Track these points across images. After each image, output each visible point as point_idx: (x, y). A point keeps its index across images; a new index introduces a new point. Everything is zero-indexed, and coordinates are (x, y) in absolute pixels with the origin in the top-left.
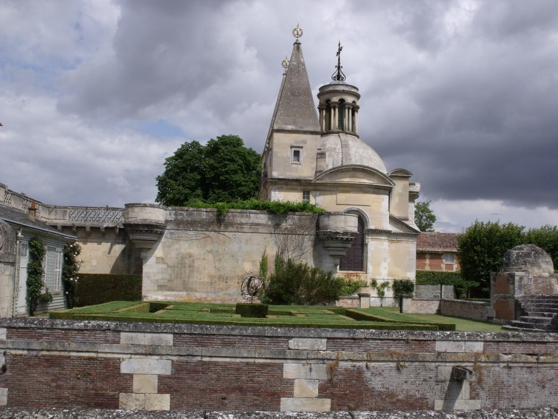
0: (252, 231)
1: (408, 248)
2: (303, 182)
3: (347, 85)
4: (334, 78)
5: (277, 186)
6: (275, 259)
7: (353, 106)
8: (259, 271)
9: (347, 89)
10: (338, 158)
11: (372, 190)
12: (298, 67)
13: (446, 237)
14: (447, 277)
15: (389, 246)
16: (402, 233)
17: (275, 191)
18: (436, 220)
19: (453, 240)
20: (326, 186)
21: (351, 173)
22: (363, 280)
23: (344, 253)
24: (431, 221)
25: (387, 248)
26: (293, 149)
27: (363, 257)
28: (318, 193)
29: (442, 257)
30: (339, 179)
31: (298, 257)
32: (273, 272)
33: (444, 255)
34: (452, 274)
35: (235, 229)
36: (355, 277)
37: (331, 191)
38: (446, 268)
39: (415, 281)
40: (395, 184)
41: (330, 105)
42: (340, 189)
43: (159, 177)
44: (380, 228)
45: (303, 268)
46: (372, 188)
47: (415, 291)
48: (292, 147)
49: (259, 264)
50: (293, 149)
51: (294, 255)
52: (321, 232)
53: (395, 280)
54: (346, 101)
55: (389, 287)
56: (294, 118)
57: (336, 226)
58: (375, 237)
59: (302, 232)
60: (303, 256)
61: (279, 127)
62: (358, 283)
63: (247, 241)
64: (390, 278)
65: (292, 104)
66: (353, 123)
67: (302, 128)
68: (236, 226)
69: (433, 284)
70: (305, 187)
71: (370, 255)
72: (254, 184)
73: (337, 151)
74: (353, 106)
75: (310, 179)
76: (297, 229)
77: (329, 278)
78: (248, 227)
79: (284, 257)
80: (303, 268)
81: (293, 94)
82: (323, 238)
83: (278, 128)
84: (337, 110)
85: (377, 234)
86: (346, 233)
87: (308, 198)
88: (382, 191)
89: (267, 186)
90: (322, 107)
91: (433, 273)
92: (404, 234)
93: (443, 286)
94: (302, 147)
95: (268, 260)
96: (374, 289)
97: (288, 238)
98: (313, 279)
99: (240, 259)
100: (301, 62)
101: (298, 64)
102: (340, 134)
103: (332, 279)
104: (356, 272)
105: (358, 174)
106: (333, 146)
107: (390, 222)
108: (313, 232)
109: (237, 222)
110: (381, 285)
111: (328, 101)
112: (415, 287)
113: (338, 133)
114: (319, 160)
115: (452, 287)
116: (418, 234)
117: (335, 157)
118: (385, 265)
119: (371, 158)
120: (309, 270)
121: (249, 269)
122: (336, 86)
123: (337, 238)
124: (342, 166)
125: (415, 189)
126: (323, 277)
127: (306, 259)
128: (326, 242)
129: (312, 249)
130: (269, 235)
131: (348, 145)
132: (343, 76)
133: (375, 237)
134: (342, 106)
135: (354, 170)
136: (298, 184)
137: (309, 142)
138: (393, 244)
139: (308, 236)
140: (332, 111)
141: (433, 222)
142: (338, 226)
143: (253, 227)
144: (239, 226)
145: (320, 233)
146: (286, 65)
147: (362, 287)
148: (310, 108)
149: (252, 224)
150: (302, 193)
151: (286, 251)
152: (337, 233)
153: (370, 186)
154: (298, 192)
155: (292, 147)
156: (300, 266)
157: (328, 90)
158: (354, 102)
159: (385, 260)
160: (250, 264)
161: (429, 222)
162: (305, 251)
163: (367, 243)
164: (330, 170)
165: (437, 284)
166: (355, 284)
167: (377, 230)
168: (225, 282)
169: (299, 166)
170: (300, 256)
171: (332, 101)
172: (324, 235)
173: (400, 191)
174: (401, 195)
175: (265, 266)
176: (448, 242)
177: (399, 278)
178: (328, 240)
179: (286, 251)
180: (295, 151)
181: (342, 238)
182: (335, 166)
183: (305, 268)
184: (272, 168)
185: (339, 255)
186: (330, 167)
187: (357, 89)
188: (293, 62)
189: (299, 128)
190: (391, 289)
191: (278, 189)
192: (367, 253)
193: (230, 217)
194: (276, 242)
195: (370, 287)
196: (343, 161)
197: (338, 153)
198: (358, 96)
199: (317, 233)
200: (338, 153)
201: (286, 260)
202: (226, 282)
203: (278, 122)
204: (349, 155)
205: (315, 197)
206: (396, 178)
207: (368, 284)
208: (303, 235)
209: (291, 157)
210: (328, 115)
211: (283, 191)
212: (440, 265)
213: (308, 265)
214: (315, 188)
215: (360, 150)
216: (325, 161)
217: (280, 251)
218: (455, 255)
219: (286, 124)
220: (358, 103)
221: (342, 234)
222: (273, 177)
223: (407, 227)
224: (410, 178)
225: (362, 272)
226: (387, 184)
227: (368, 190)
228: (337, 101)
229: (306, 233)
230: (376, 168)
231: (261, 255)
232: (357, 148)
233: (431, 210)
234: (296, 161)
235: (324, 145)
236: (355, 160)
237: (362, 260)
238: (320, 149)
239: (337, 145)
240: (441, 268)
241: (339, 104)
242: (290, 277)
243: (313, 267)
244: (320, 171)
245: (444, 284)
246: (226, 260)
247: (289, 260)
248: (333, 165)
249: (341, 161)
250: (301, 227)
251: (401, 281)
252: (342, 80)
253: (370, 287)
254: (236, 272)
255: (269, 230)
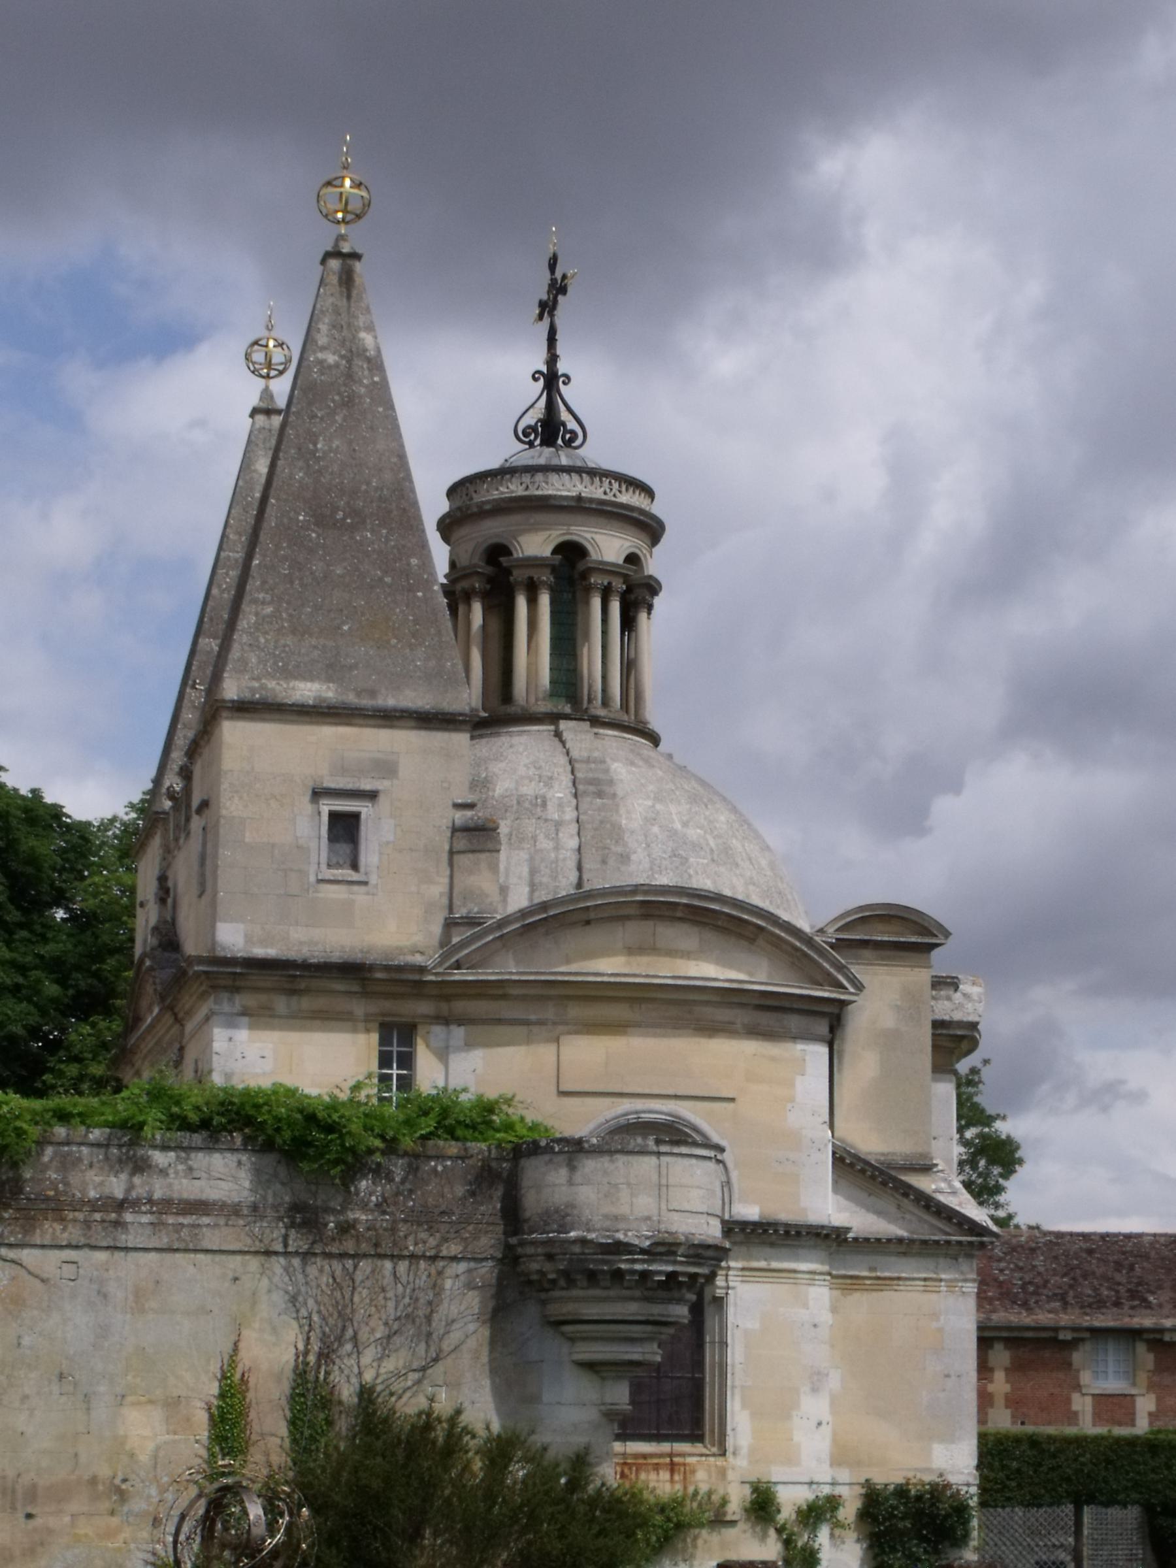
0: (164, 1241)
1: (935, 1316)
2: (379, 975)
3: (595, 473)
4: (525, 435)
5: (240, 1001)
6: (286, 1387)
7: (626, 578)
8: (204, 1453)
9: (594, 491)
10: (557, 848)
11: (742, 1017)
12: (350, 376)
13: (1090, 1252)
14: (1109, 1462)
15: (834, 1310)
16: (900, 1240)
17: (231, 1025)
18: (1020, 1161)
19: (1131, 1268)
20: (504, 997)
21: (634, 931)
22: (704, 1488)
23: (653, 1353)
24: (996, 1170)
25: (826, 1317)
26: (327, 806)
27: (702, 1371)
28: (458, 1033)
29: (1077, 1357)
30: (568, 961)
31: (415, 1376)
32: (280, 1458)
33: (1088, 1346)
34: (1132, 1442)
35: (74, 1233)
36: (665, 1475)
37: (526, 1023)
38: (1098, 1417)
39: (974, 1490)
40: (859, 987)
41: (508, 572)
42: (575, 1011)
43: (482, 1095)
44: (785, 1215)
45: (439, 1434)
46: (742, 1005)
47: (974, 1543)
48: (318, 794)
49: (202, 1417)
50: (327, 806)
51: (389, 1365)
52: (534, 1243)
53: (868, 1483)
54: (594, 555)
55: (837, 1525)
56: (331, 643)
57: (614, 1210)
58: (762, 1264)
59: (432, 1242)
60: (437, 1371)
61: (253, 690)
62: (677, 1503)
63: (139, 1295)
64: (844, 1475)
65: (318, 567)
66: (630, 666)
67: (373, 693)
68: (80, 1216)
69: (1034, 1502)
70: (387, 1005)
71: (736, 1354)
72: (62, 982)
73: (553, 813)
74: (626, 578)
75: (418, 959)
76: (403, 1229)
77: (575, 1484)
78: (145, 1219)
79: (335, 1377)
80: (439, 1434)
81: (322, 520)
82: (542, 1273)
83: (247, 695)
84: (545, 600)
85: (772, 1245)
86: (664, 1248)
87: (407, 1061)
88: (794, 1022)
89: (186, 1002)
90: (464, 584)
91: (1033, 1442)
92: (912, 1241)
93: (1088, 1512)
94: (372, 796)
95: (250, 1395)
96: (764, 1537)
97: (359, 1276)
98: (492, 1489)
99: (102, 1389)
100: (362, 353)
101: (349, 361)
102: (563, 725)
103: (591, 1489)
104: (665, 1447)
105: (668, 933)
106: (529, 790)
107: (835, 1182)
108: (488, 1242)
109: (84, 1191)
110: (799, 1512)
111: (497, 552)
112: (975, 1523)
113: (554, 718)
114: (463, 860)
115: (1129, 1516)
116: (982, 1245)
117: (545, 844)
118: (815, 1406)
119: (726, 850)
120: (473, 1444)
121: (150, 1446)
122: (539, 477)
123: (618, 1275)
124: (581, 893)
125: (961, 1006)
126: (543, 1472)
127: (453, 1385)
128: (557, 1293)
129: (486, 1332)
130: (254, 1263)
131: (611, 782)
132: (572, 425)
133: (762, 1264)
134: (571, 582)
135: (646, 917)
136: (355, 988)
137: (406, 768)
138: (857, 1295)
139: (462, 1267)
140: (521, 604)
141: (1008, 1172)
142: (624, 1209)
143: (171, 1220)
144: (98, 1216)
145: (530, 1250)
146: (269, 365)
147: (701, 1525)
148: (411, 589)
149: (166, 1205)
150: (375, 1037)
151: (348, 1347)
152: (620, 1248)
153: (732, 996)
154: (355, 1030)
155: (318, 794)
156: (426, 1423)
157: (495, 495)
158: (632, 559)
159: (816, 1380)
160: (157, 1414)
161: (985, 1175)
162: (446, 1346)
163: (719, 1292)
164: (523, 913)
165: (1056, 1502)
166: (662, 1510)
167: (774, 1225)
168: (21, 1516)
169: (360, 896)
170: (423, 1369)
171: (518, 554)
172: (550, 1257)
173: (889, 1021)
174: (889, 1041)
175: (234, 1425)
176: (1105, 1278)
177: (888, 1476)
178: (571, 1283)
179: (348, 1347)
180: (334, 816)
181: (645, 1275)
182: (543, 896)
183: (450, 1435)
184: (213, 904)
185: (632, 1363)
186: (519, 900)
187: (648, 492)
188: (323, 349)
189: (359, 694)
190: (851, 1536)
191: (245, 1013)
192: (724, 1344)
193: (46, 1167)
194: (293, 1299)
195: (741, 1526)
196: (586, 866)
197: (558, 825)
198: (652, 530)
199: (508, 1247)
200: (558, 825)
201: (347, 1393)
202: (29, 1516)
203: (244, 661)
204: (617, 833)
205: (443, 1055)
206: (867, 953)
207: (734, 1508)
208: (434, 1258)
209: (313, 845)
210: (495, 626)
211: (272, 1028)
212: (1068, 1401)
213: (464, 1419)
214: (444, 1007)
215: (673, 809)
216: (494, 868)
217: (315, 1346)
218: (1141, 1348)
219: (288, 674)
220: (656, 564)
221: (643, 1251)
222: (220, 953)
223: (927, 1207)
224: (935, 953)
225: (699, 1448)
226: (818, 984)
227: (723, 1015)
228: (546, 551)
229: (454, 1249)
230: (756, 900)
231: (215, 1368)
232: (658, 798)
233: (991, 1111)
234: (338, 866)
235: (480, 784)
236: (646, 864)
237: (698, 1387)
238: (470, 806)
239: (549, 781)
240: (1072, 1417)
241: (554, 569)
242: (376, 1484)
243: (496, 1427)
244: (471, 922)
245: (1091, 1500)
246: (25, 1398)
247: (366, 1394)
248: (533, 887)
249: (571, 864)
250: (426, 1218)
251: (901, 1492)
252: (568, 443)
253: (741, 1526)
254: (83, 1458)
255: (251, 1235)
